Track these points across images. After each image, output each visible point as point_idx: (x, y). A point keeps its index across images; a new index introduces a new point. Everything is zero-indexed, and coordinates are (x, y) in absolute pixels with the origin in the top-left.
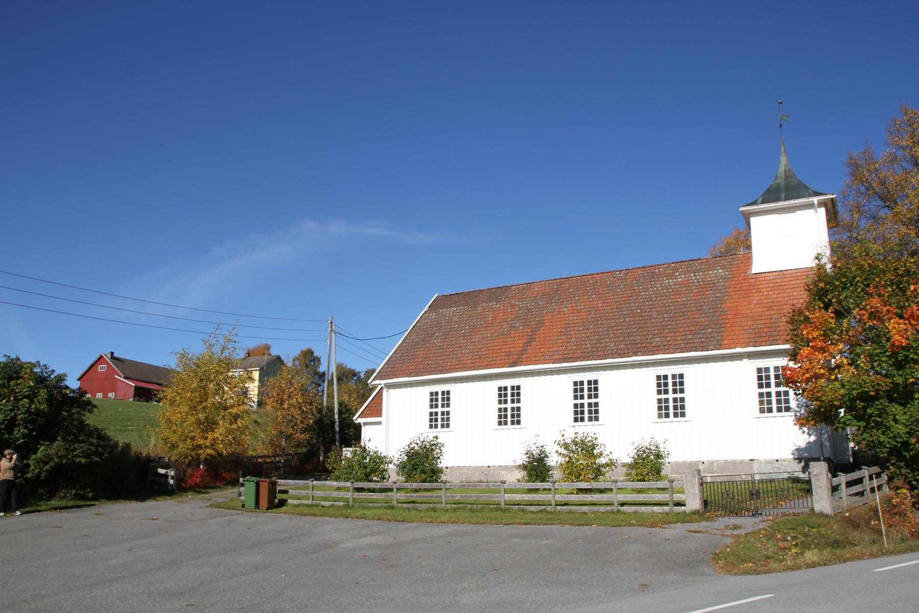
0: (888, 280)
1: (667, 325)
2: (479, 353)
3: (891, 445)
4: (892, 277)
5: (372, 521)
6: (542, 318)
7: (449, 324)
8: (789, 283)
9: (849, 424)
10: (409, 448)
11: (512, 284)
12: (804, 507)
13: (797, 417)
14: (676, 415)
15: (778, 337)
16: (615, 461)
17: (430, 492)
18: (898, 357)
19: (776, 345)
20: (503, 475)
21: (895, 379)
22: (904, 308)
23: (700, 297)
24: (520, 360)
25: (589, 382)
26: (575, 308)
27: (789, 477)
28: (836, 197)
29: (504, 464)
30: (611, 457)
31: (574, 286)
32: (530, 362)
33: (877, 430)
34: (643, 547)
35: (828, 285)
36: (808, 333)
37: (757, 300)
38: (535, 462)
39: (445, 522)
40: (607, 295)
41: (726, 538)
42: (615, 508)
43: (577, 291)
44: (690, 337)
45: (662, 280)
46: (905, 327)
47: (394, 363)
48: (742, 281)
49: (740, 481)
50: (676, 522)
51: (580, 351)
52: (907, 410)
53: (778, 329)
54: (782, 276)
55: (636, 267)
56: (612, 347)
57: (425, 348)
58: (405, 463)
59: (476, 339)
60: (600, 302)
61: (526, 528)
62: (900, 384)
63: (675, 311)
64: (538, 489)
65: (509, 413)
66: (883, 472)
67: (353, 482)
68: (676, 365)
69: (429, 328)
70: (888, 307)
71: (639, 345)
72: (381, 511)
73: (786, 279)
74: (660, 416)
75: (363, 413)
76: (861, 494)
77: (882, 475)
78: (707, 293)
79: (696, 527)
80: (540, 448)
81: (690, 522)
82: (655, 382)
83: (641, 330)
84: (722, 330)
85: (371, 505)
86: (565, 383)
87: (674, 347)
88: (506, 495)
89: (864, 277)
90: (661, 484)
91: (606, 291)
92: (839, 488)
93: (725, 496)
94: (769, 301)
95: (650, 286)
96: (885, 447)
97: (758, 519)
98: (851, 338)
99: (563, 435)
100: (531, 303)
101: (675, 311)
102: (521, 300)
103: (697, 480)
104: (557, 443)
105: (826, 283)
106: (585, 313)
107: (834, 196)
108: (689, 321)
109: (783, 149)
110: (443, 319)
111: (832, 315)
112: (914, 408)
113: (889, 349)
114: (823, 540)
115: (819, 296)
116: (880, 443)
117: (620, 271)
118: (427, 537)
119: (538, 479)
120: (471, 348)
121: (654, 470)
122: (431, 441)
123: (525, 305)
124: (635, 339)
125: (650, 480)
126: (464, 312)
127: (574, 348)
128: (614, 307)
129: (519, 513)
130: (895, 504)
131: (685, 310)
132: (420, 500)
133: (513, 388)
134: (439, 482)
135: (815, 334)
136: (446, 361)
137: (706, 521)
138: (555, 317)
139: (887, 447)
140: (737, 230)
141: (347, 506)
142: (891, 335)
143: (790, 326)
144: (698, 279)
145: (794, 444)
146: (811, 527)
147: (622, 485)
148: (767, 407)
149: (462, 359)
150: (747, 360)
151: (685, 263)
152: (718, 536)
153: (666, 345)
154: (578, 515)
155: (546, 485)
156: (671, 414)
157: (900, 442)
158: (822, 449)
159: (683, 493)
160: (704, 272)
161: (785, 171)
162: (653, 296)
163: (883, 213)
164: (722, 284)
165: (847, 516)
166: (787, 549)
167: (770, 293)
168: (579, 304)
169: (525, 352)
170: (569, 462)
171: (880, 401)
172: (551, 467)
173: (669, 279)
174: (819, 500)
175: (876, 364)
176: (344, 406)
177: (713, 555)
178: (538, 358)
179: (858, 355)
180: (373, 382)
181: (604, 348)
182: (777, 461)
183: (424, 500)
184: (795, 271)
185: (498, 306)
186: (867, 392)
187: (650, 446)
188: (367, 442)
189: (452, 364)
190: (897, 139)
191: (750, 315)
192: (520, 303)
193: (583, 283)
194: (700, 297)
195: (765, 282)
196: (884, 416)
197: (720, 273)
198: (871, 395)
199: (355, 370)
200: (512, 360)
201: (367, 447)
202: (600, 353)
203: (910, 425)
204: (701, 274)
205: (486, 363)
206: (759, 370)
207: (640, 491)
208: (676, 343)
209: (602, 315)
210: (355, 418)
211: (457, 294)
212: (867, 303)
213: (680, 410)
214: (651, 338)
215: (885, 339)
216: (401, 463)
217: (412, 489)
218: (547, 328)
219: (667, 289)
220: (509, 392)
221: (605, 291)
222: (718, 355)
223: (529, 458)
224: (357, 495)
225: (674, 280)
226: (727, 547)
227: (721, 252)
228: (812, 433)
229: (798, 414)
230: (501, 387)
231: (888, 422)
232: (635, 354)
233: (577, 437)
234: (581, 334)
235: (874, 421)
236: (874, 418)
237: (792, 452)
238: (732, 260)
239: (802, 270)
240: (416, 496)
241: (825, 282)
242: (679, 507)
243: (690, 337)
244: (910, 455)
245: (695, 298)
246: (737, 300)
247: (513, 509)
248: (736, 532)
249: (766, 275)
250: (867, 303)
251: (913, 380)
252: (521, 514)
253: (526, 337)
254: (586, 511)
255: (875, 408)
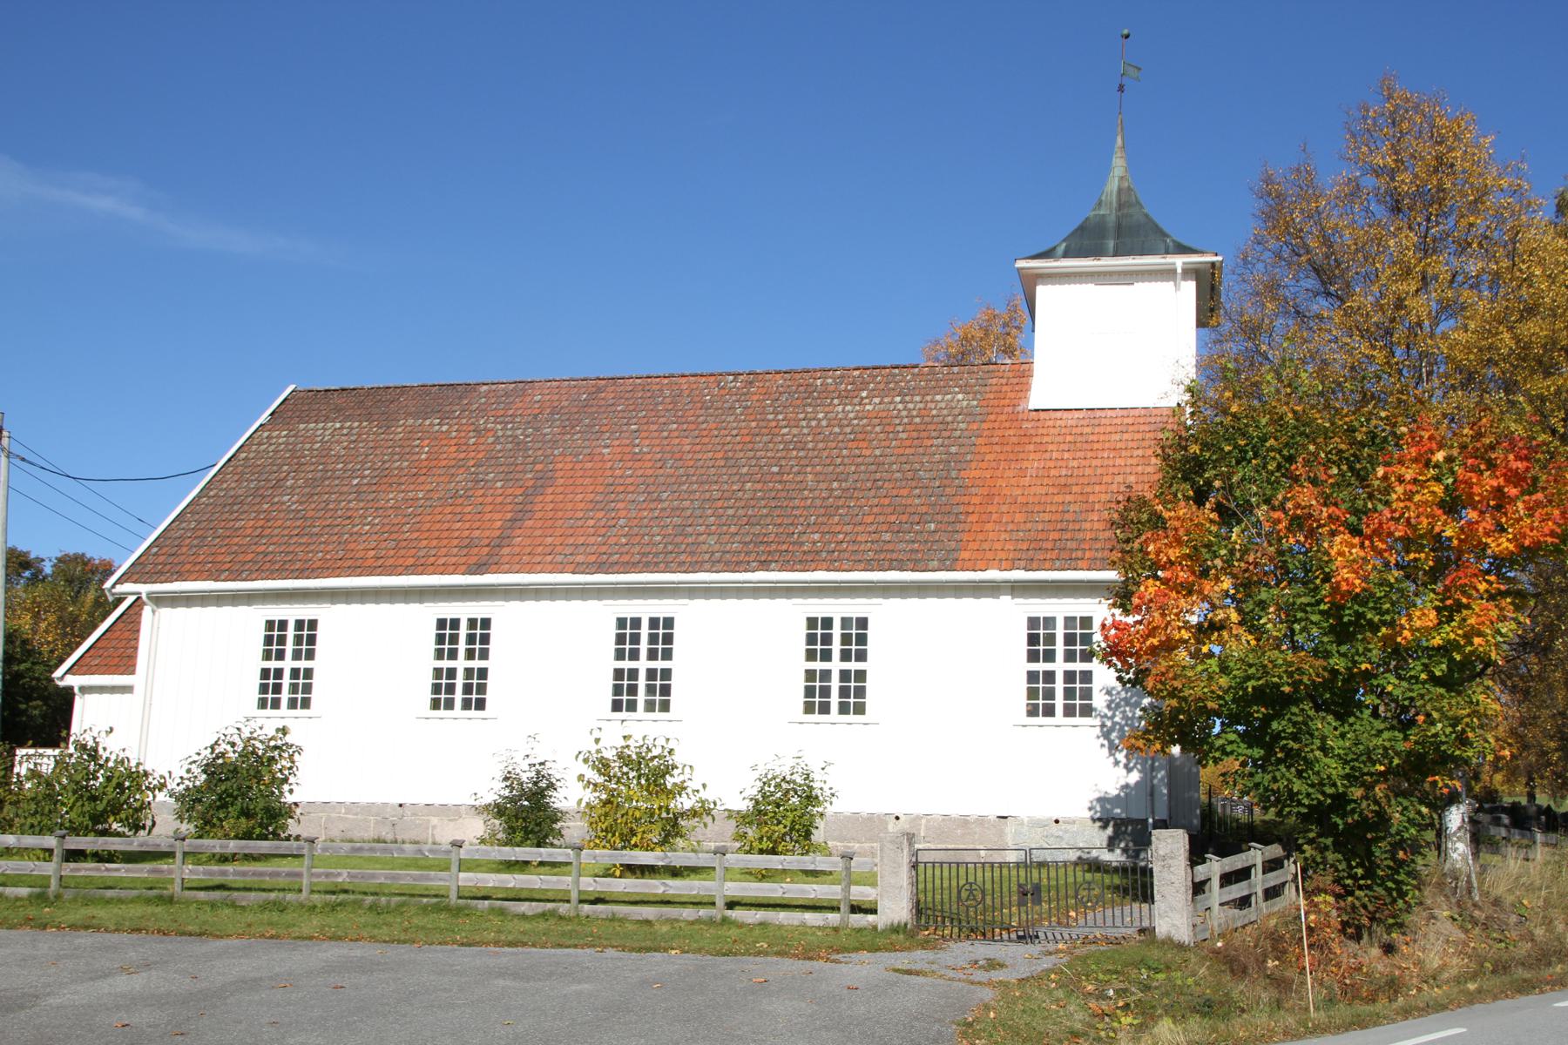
0: (1334, 452)
1: (838, 508)
2: (394, 536)
3: (1313, 800)
4: (1343, 447)
5: (116, 935)
6: (551, 467)
7: (323, 460)
8: (1107, 438)
9: (1232, 752)
10: (212, 753)
11: (480, 381)
12: (1114, 927)
13: (1105, 729)
14: (844, 709)
15: (1080, 554)
16: (712, 806)
17: (258, 864)
18: (1343, 616)
19: (1075, 569)
20: (434, 827)
21: (1332, 661)
22: (1365, 513)
23: (912, 451)
24: (496, 559)
25: (654, 623)
26: (627, 450)
27: (1080, 858)
28: (1222, 262)
29: (437, 800)
30: (703, 795)
31: (627, 399)
32: (518, 566)
33: (1288, 768)
34: (803, 1005)
35: (1209, 450)
36: (1158, 552)
37: (1038, 468)
38: (526, 800)
39: (311, 938)
40: (704, 426)
41: (978, 988)
42: (717, 913)
43: (634, 410)
44: (887, 537)
45: (829, 405)
46: (1362, 554)
47: (176, 543)
48: (1007, 425)
49: (975, 863)
50: (856, 950)
51: (637, 549)
52: (1347, 728)
53: (1080, 536)
54: (1093, 422)
55: (771, 369)
56: (710, 545)
57: (259, 513)
58: (198, 789)
59: (388, 500)
60: (688, 441)
61: (512, 954)
62: (1341, 674)
63: (856, 477)
64: (527, 863)
65: (460, 681)
66: (1288, 857)
67: (63, 837)
68: (870, 598)
69: (272, 464)
70: (1332, 509)
71: (774, 547)
72: (136, 911)
73: (1102, 429)
74: (1033, 712)
75: (81, 663)
76: (1244, 902)
77: (1286, 861)
78: (929, 443)
79: (907, 962)
80: (537, 766)
81: (887, 950)
82: (432, 631)
83: (778, 512)
84: (959, 527)
85: (109, 893)
86: (600, 618)
87: (853, 558)
88: (462, 875)
89: (1284, 439)
90: (824, 863)
91: (701, 419)
92: (1207, 888)
93: (964, 895)
94: (1064, 472)
95: (802, 416)
96: (1300, 804)
97: (1033, 949)
98: (1251, 567)
99: (597, 741)
100: (525, 429)
101: (856, 477)
102: (502, 419)
103: (905, 859)
104: (581, 757)
105: (1205, 446)
106: (650, 464)
107: (1219, 258)
108: (887, 501)
109: (1119, 140)
110: (307, 446)
111: (1214, 516)
112: (1361, 725)
113: (1326, 597)
114: (1182, 998)
115: (1184, 471)
116: (1292, 795)
117: (736, 375)
118: (277, 975)
119: (528, 839)
120: (376, 521)
121: (798, 831)
122: (271, 739)
123: (509, 433)
124: (764, 531)
125: (787, 850)
126: (360, 435)
127: (624, 540)
128: (720, 455)
129: (491, 917)
130: (1313, 925)
131: (878, 476)
132: (239, 881)
133: (654, 623)
134: (282, 840)
135: (1174, 553)
136: (312, 547)
137: (924, 948)
138: (581, 465)
139: (1304, 805)
140: (988, 309)
141: (41, 898)
142: (1334, 568)
143: (1118, 531)
144: (910, 410)
145: (1094, 788)
146: (1154, 969)
147: (738, 860)
148: (1039, 703)
149: (352, 546)
150: (1010, 597)
151: (883, 372)
152: (960, 984)
153: (833, 552)
154: (630, 927)
155: (561, 854)
156: (458, 703)
157: (1330, 796)
158: (1152, 801)
159: (874, 885)
160: (924, 396)
161: (1120, 190)
162: (809, 439)
163: (1321, 305)
164: (963, 426)
165: (1220, 948)
166: (1107, 1015)
167: (1066, 455)
168: (637, 441)
169: (506, 542)
170: (608, 802)
171: (1301, 706)
172: (561, 812)
173: (846, 404)
174: (1166, 912)
175: (1297, 627)
176: (18, 643)
177: (959, 1025)
178: (538, 559)
179: (1263, 605)
180: (118, 586)
181: (694, 548)
182: (1057, 821)
183: (249, 881)
184: (1121, 413)
185: (445, 428)
186: (1277, 686)
187: (792, 774)
188: (103, 734)
189: (328, 557)
190: (1364, 149)
191: (1020, 500)
192: (499, 427)
193: (649, 395)
194: (912, 451)
195: (1056, 431)
196: (1305, 738)
197: (959, 401)
198: (1283, 692)
199: (28, 553)
200: (477, 558)
201: (101, 751)
202: (683, 557)
203: (1353, 760)
204: (918, 398)
205: (411, 561)
206: (1033, 622)
207: (764, 875)
208: (855, 548)
209: (692, 471)
210: (58, 673)
211: (343, 390)
212: (1289, 495)
213: (854, 697)
214: (800, 533)
215: (1321, 576)
216: (187, 789)
217: (214, 855)
218: (561, 489)
219: (841, 426)
220: (463, 631)
221: (699, 416)
222: (947, 582)
223: (511, 787)
224: (69, 868)
225: (857, 408)
226: (987, 1008)
227: (949, 356)
228: (1135, 766)
229: (1109, 723)
230: (445, 620)
231: (1312, 751)
232: (764, 565)
233: (628, 746)
234: (640, 510)
235: (1283, 749)
236: (1285, 742)
237: (1090, 805)
238: (987, 375)
239: (1136, 413)
240: (236, 873)
241: (1201, 444)
242: (862, 915)
243: (887, 537)
244: (1346, 824)
245: (901, 451)
246: (994, 464)
247: (477, 909)
248: (998, 975)
249: (1058, 414)
250: (1289, 495)
251: (1369, 666)
252: (496, 921)
253: (510, 507)
254: (650, 918)
255: (1290, 720)
